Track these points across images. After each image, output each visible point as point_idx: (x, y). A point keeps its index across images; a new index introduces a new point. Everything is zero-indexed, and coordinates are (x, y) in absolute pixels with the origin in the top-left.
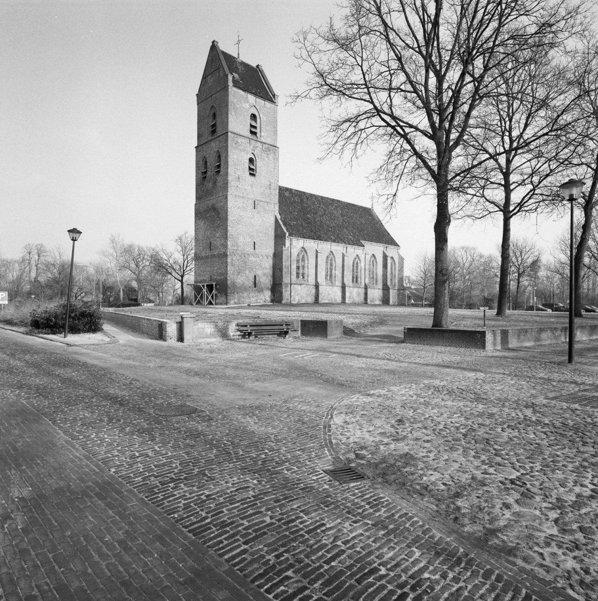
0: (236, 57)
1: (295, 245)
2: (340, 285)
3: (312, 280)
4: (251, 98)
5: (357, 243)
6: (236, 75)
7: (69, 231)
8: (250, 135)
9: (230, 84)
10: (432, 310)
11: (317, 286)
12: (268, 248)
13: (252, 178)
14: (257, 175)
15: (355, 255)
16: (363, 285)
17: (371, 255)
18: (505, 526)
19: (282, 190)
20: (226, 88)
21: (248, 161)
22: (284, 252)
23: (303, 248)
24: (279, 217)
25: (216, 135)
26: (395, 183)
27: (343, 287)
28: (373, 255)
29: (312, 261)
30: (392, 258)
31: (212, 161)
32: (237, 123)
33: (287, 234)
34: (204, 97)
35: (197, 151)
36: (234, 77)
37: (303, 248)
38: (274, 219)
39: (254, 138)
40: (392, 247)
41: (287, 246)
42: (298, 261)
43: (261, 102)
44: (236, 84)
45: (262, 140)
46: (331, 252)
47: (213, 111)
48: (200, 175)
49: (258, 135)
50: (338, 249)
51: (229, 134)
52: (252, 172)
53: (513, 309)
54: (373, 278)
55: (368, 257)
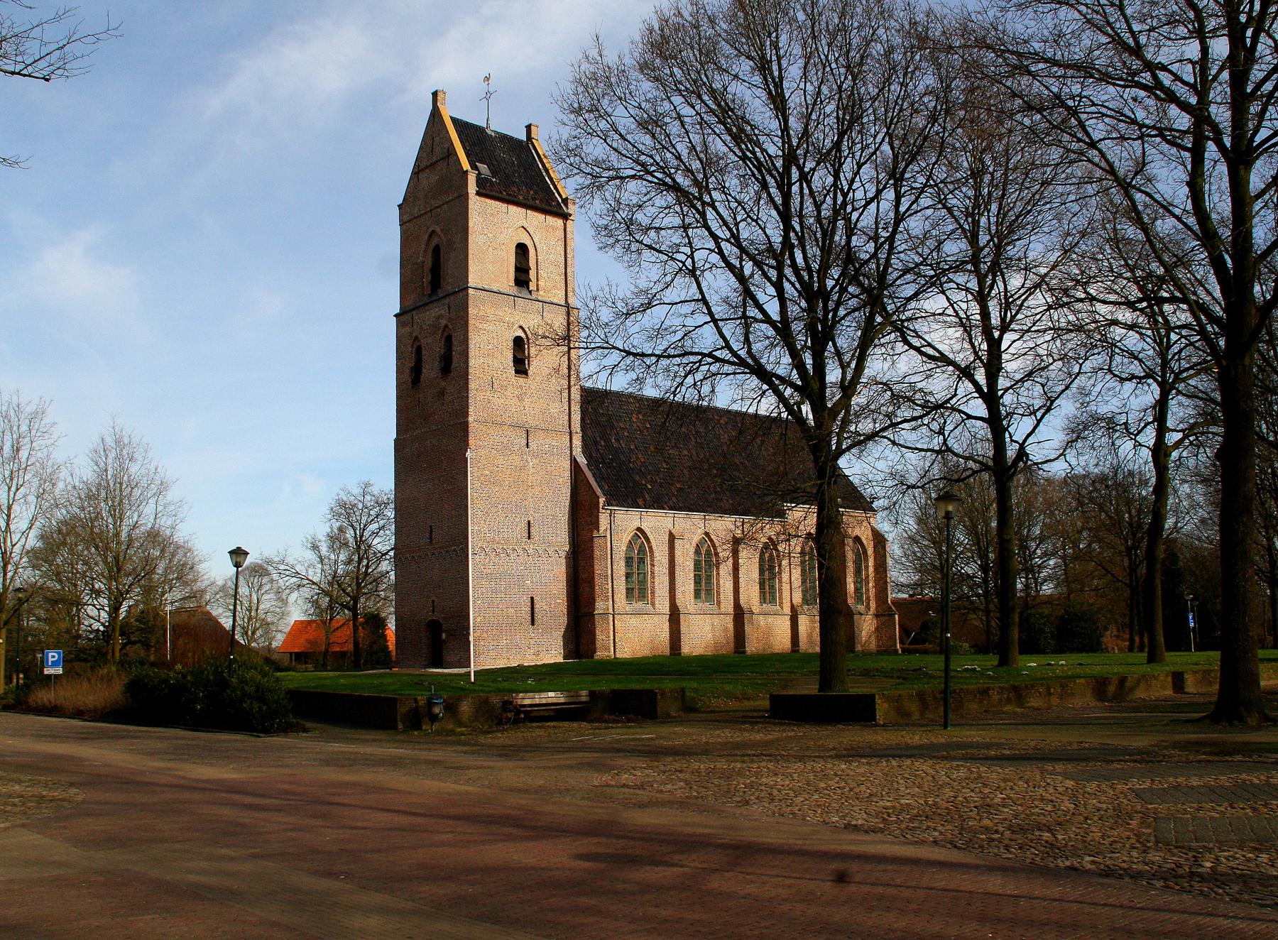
1: (620, 525)
2: (667, 610)
3: (663, 606)
4: (516, 214)
6: (483, 168)
7: (231, 553)
8: (514, 290)
9: (472, 188)
10: (1216, 655)
11: (675, 616)
13: (521, 380)
16: (787, 610)
20: (464, 197)
21: (511, 344)
24: (582, 460)
25: (441, 293)
26: (690, 19)
27: (675, 616)
30: (857, 539)
32: (487, 264)
33: (602, 500)
34: (416, 212)
35: (400, 325)
37: (639, 529)
38: (567, 465)
39: (525, 294)
41: (602, 529)
42: (629, 561)
43: (535, 220)
44: (485, 190)
46: (707, 534)
47: (435, 242)
48: (407, 372)
49: (532, 286)
51: (471, 291)
52: (521, 366)
53: (652, 691)
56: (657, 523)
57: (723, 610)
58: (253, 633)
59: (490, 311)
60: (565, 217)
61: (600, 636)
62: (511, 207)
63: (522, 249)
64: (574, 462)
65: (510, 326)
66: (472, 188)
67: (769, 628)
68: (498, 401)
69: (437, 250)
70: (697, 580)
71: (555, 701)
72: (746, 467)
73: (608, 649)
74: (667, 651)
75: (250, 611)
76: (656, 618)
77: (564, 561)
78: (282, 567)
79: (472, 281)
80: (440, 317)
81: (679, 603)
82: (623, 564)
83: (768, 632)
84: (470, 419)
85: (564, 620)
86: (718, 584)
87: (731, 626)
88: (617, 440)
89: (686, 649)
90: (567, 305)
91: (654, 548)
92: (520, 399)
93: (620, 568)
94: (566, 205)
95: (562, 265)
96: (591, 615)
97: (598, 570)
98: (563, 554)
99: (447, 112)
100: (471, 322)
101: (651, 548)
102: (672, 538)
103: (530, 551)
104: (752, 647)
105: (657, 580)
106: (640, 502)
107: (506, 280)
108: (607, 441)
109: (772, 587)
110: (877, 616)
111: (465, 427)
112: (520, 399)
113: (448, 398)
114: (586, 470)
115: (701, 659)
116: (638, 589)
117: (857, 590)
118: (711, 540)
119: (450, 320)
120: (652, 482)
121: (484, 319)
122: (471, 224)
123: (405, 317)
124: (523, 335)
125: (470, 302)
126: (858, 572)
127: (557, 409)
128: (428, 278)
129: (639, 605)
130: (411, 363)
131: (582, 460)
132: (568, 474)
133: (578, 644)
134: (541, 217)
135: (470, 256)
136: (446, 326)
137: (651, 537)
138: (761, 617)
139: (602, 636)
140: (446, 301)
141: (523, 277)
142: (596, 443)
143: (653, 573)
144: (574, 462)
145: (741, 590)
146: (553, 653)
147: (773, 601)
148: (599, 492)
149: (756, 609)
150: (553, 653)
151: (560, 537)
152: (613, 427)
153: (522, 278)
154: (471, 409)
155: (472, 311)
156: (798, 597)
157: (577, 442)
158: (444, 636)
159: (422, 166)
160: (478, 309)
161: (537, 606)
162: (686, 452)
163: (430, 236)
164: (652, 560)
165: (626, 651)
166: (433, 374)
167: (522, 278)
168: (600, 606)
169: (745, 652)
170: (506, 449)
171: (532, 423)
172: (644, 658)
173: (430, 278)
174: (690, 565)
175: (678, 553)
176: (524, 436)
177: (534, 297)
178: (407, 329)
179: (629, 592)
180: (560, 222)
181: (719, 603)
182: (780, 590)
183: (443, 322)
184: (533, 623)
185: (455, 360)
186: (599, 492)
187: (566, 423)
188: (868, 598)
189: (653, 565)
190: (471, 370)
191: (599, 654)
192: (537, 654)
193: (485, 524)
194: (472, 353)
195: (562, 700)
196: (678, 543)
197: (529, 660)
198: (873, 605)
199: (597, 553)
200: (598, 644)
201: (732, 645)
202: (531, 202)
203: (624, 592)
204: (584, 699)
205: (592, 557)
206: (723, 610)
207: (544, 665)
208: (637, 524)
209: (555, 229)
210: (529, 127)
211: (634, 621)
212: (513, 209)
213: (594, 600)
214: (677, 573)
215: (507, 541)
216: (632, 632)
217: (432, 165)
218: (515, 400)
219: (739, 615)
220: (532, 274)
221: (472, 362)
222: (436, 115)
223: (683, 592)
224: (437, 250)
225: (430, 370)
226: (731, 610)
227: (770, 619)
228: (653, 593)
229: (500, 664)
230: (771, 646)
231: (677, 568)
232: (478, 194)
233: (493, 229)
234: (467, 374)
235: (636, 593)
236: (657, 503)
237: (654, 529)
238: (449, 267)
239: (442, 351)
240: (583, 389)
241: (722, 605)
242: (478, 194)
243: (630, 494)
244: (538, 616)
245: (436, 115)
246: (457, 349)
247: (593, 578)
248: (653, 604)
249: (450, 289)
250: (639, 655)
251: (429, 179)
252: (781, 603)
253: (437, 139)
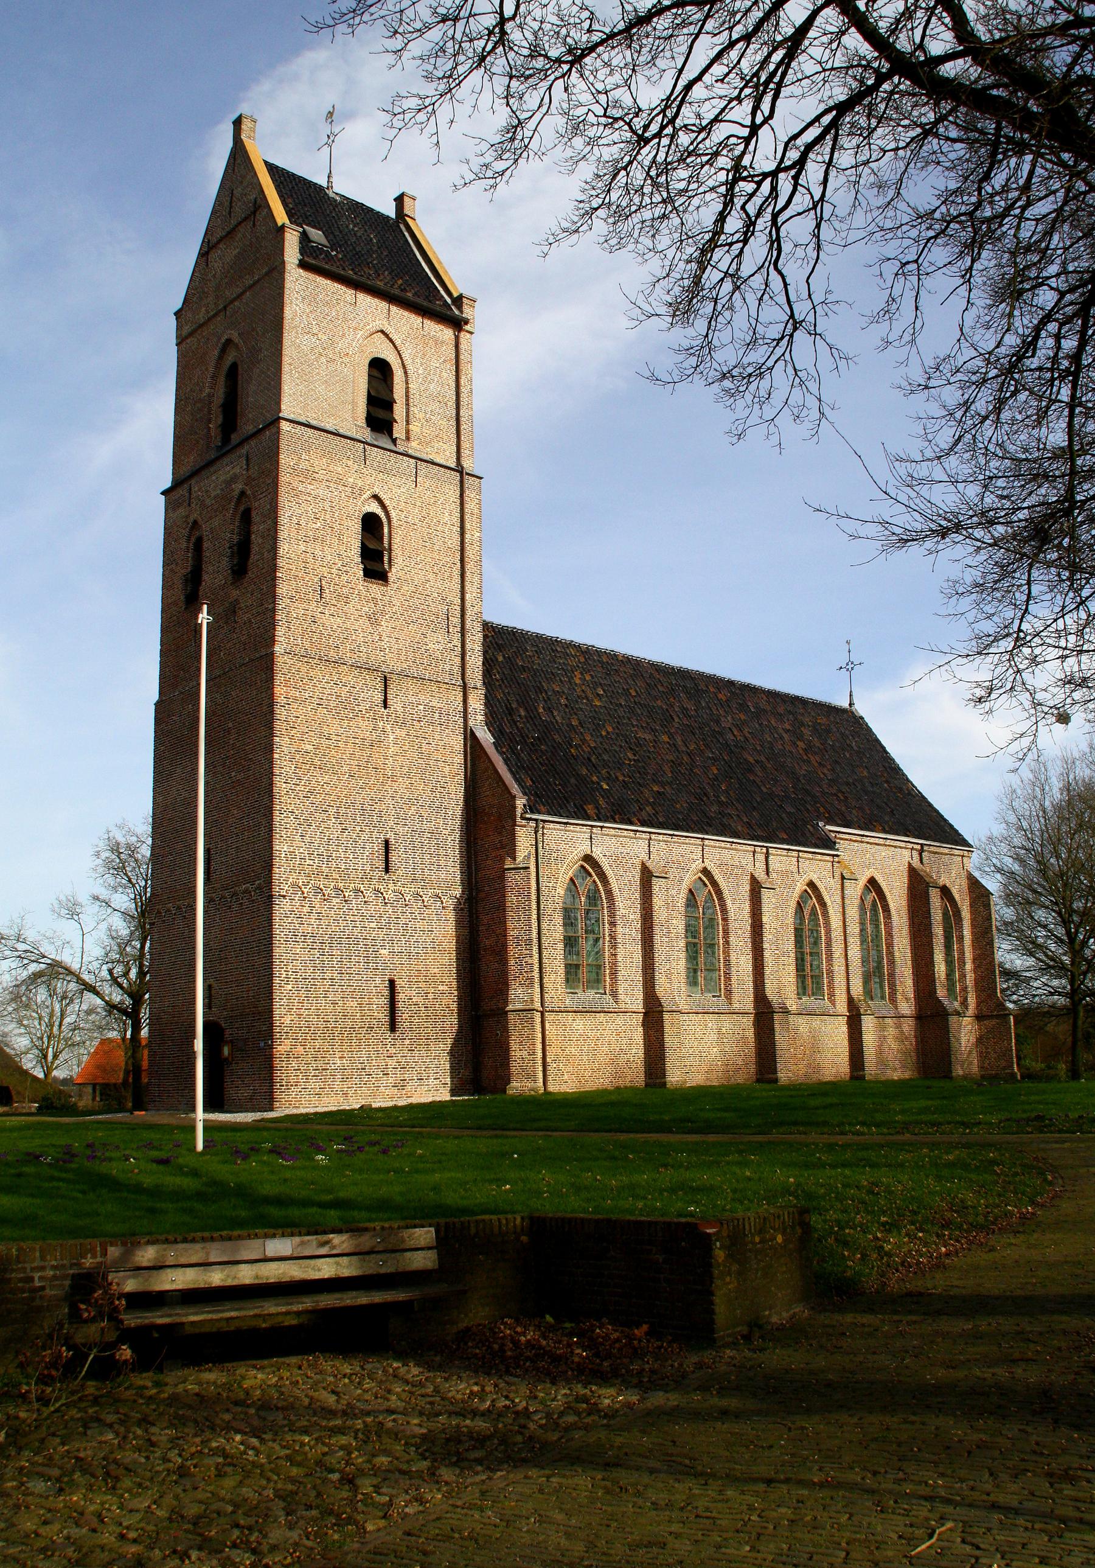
0: (325, 185)
1: (555, 849)
2: (638, 1005)
3: (633, 998)
5: (803, 832)
8: (367, 434)
9: (292, 253)
11: (653, 1016)
12: (438, 870)
13: (375, 589)
14: (392, 576)
15: (800, 886)
16: (842, 1007)
17: (863, 881)
18: (956, 1147)
19: (499, 640)
20: (277, 270)
22: (512, 878)
23: (588, 858)
24: (485, 737)
27: (653, 1016)
28: (872, 881)
29: (628, 907)
30: (945, 891)
31: (221, 533)
33: (520, 802)
34: (201, 317)
35: (170, 507)
36: (304, 238)
37: (588, 858)
38: (457, 742)
40: (945, 848)
41: (521, 855)
43: (404, 323)
45: (414, 448)
46: (705, 871)
47: (229, 359)
48: (179, 584)
49: (398, 431)
50: (732, 859)
51: (285, 426)
52: (375, 562)
54: (877, 972)
55: (855, 890)
56: (621, 848)
57: (736, 1006)
58: (55, 1057)
59: (320, 463)
60: (458, 324)
61: (517, 1052)
62: (361, 296)
63: (380, 369)
64: (470, 737)
65: (356, 492)
66: (292, 253)
67: (815, 1036)
68: (331, 622)
69: (233, 373)
70: (692, 952)
71: (295, 1272)
72: (764, 768)
73: (532, 1077)
74: (640, 1080)
75: (51, 1025)
76: (620, 1019)
77: (451, 916)
78: (21, 947)
79: (288, 408)
80: (234, 479)
81: (660, 991)
82: (559, 919)
83: (815, 1047)
84: (278, 649)
85: (452, 1022)
86: (727, 961)
87: (750, 1034)
88: (549, 710)
89: (675, 1076)
90: (460, 470)
91: (616, 892)
92: (373, 619)
93: (555, 931)
94: (460, 308)
95: (452, 403)
96: (501, 1014)
97: (514, 928)
98: (450, 903)
99: (260, 152)
100: (284, 478)
101: (609, 893)
102: (647, 876)
103: (390, 895)
104: (787, 1071)
105: (621, 952)
106: (590, 809)
107: (352, 416)
108: (531, 711)
109: (279, 1201)
110: (979, 1018)
111: (267, 664)
112: (373, 619)
113: (243, 617)
114: (492, 752)
115: (700, 1094)
116: (586, 970)
117: (949, 975)
118: (714, 884)
119: (249, 480)
120: (608, 779)
121: (309, 475)
122: (288, 312)
123: (182, 491)
124: (379, 511)
125: (283, 444)
126: (948, 947)
127: (441, 644)
128: (217, 419)
129: (590, 995)
130: (185, 568)
131: (485, 737)
132: (459, 759)
133: (477, 1067)
134: (416, 320)
135: (286, 368)
136: (243, 493)
137: (609, 873)
138: (801, 1020)
139: (521, 1052)
140: (243, 451)
141: (381, 414)
142: (510, 711)
143: (613, 937)
144: (470, 737)
145: (767, 971)
146: (430, 1083)
147: (818, 991)
148: (515, 789)
149: (792, 1005)
150: (430, 1083)
151: (447, 874)
152: (540, 690)
153: (380, 414)
154: (280, 632)
155: (285, 459)
156: (857, 989)
157: (477, 703)
158: (226, 1051)
159: (214, 240)
160: (294, 455)
161: (401, 997)
162: (665, 738)
163: (223, 351)
164: (612, 914)
165: (565, 1080)
166: (220, 580)
167: (380, 414)
168: (518, 996)
169: (776, 1080)
170: (346, 707)
171: (394, 664)
172: (604, 1092)
173: (220, 420)
174: (679, 925)
175: (658, 902)
176: (380, 686)
177: (400, 448)
178: (182, 511)
179: (572, 972)
180: (448, 333)
181: (729, 993)
182: (830, 972)
183: (238, 487)
184: (393, 1027)
185: (255, 548)
186: (515, 789)
187: (457, 670)
188: (964, 989)
189: (613, 924)
190: (281, 562)
191: (517, 1086)
192: (400, 1085)
193: (301, 846)
194: (283, 534)
195: (346, 1268)
196: (657, 885)
197: (384, 1096)
198: (972, 1000)
199: (512, 899)
200: (515, 1067)
201: (753, 1068)
202: (396, 292)
203: (561, 970)
204: (422, 1260)
205: (501, 907)
206: (736, 1006)
207: (411, 1107)
208: (584, 848)
209: (438, 342)
210: (400, 200)
211: (579, 1024)
212: (365, 300)
213: (506, 985)
214: (657, 939)
215: (345, 874)
216: (576, 1047)
217: (229, 233)
218: (364, 623)
219: (765, 1014)
220: (399, 411)
221: (284, 548)
222: (239, 156)
223: (669, 976)
224: (233, 373)
225: (216, 572)
226: (749, 1006)
227: (816, 1022)
228: (614, 974)
229: (330, 1103)
230: (818, 1068)
231: (657, 930)
232: (303, 265)
233: (327, 334)
234: (274, 568)
235: (584, 974)
236: (619, 812)
237: (617, 859)
238: (251, 395)
239: (236, 538)
240: (487, 626)
241: (736, 997)
242: (303, 265)
243: (569, 796)
244: (403, 1016)
245: (239, 156)
246: (258, 527)
247: (504, 946)
248: (614, 994)
249: (250, 429)
250: (591, 1086)
251: (227, 254)
252: (832, 995)
253: (238, 192)
